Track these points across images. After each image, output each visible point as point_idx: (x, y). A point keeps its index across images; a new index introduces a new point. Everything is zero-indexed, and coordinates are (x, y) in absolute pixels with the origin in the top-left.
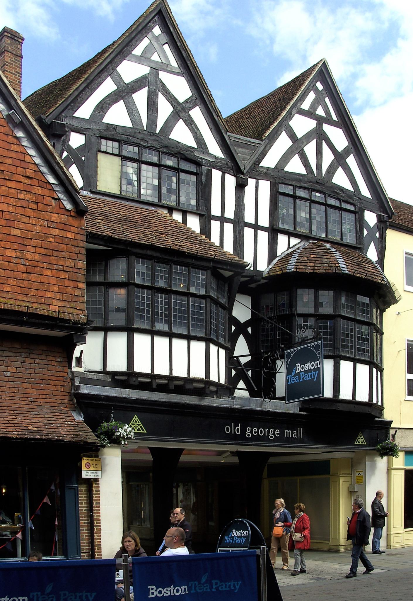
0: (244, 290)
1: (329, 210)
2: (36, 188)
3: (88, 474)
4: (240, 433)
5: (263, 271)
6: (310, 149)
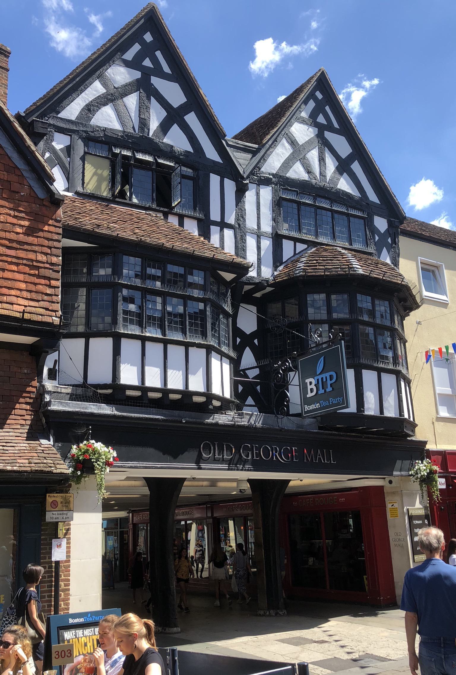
0: (248, 298)
1: (336, 216)
2: (2, 172)
6: (313, 155)
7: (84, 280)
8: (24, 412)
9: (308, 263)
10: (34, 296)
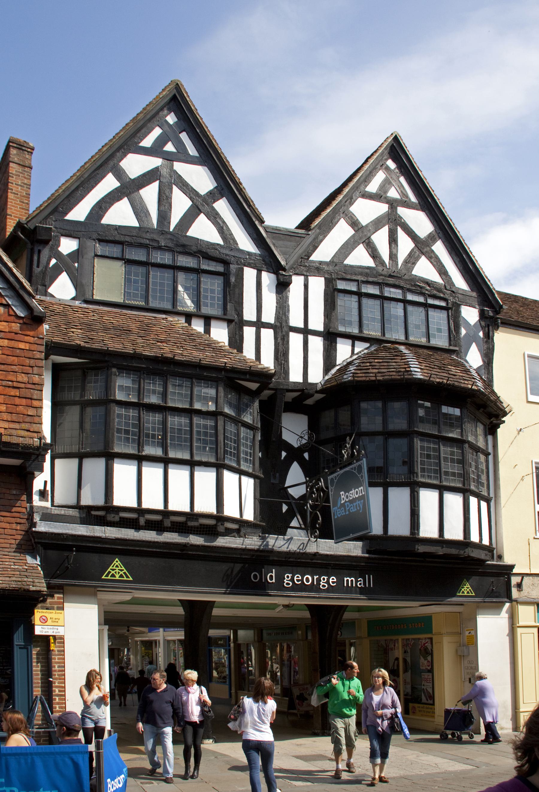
1: (410, 308)
3: (44, 630)
4: (274, 581)
5: (317, 384)
6: (380, 239)
7: (78, 398)
8: (14, 532)
9: (360, 366)
10: (14, 417)
